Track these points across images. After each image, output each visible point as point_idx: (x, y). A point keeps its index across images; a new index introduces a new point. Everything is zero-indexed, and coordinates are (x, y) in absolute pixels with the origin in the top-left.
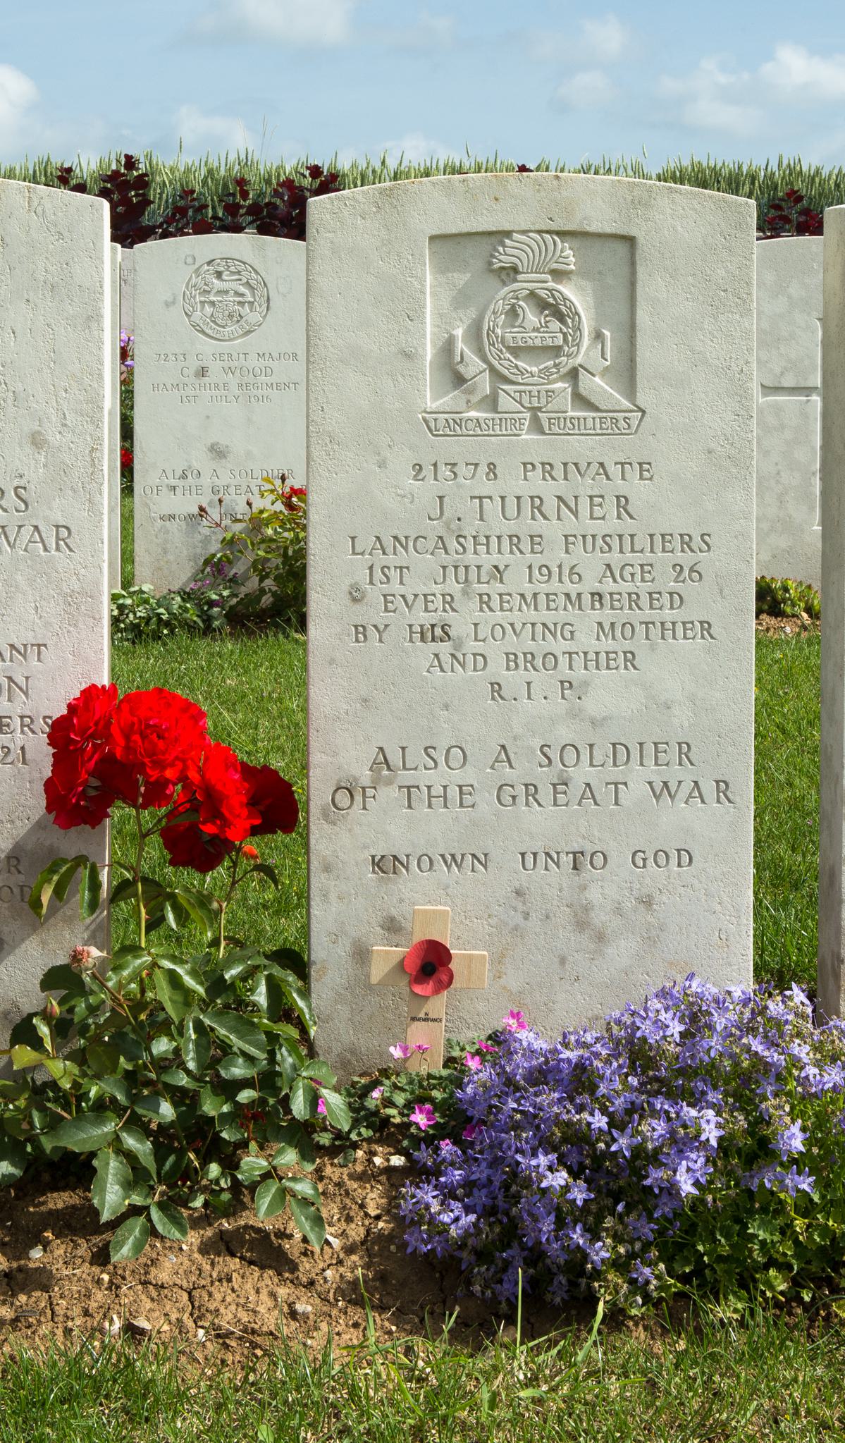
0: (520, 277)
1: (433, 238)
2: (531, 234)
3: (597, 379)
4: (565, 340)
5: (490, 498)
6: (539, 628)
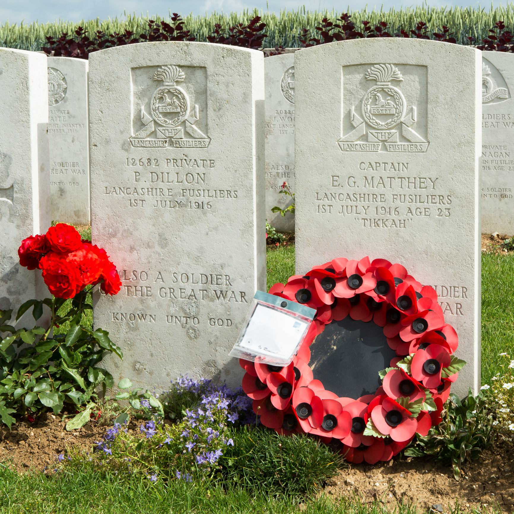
0: (378, 83)
1: (344, 67)
2: (381, 65)
4: (181, 109)
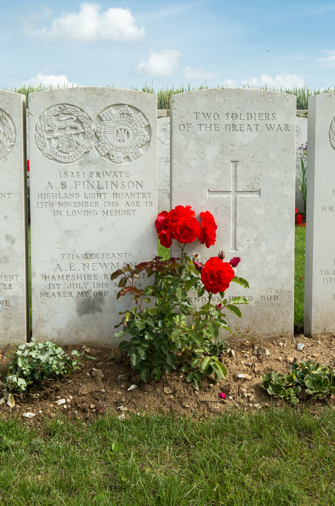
3: (115, 113)
5: (123, 172)
6: (56, 212)
